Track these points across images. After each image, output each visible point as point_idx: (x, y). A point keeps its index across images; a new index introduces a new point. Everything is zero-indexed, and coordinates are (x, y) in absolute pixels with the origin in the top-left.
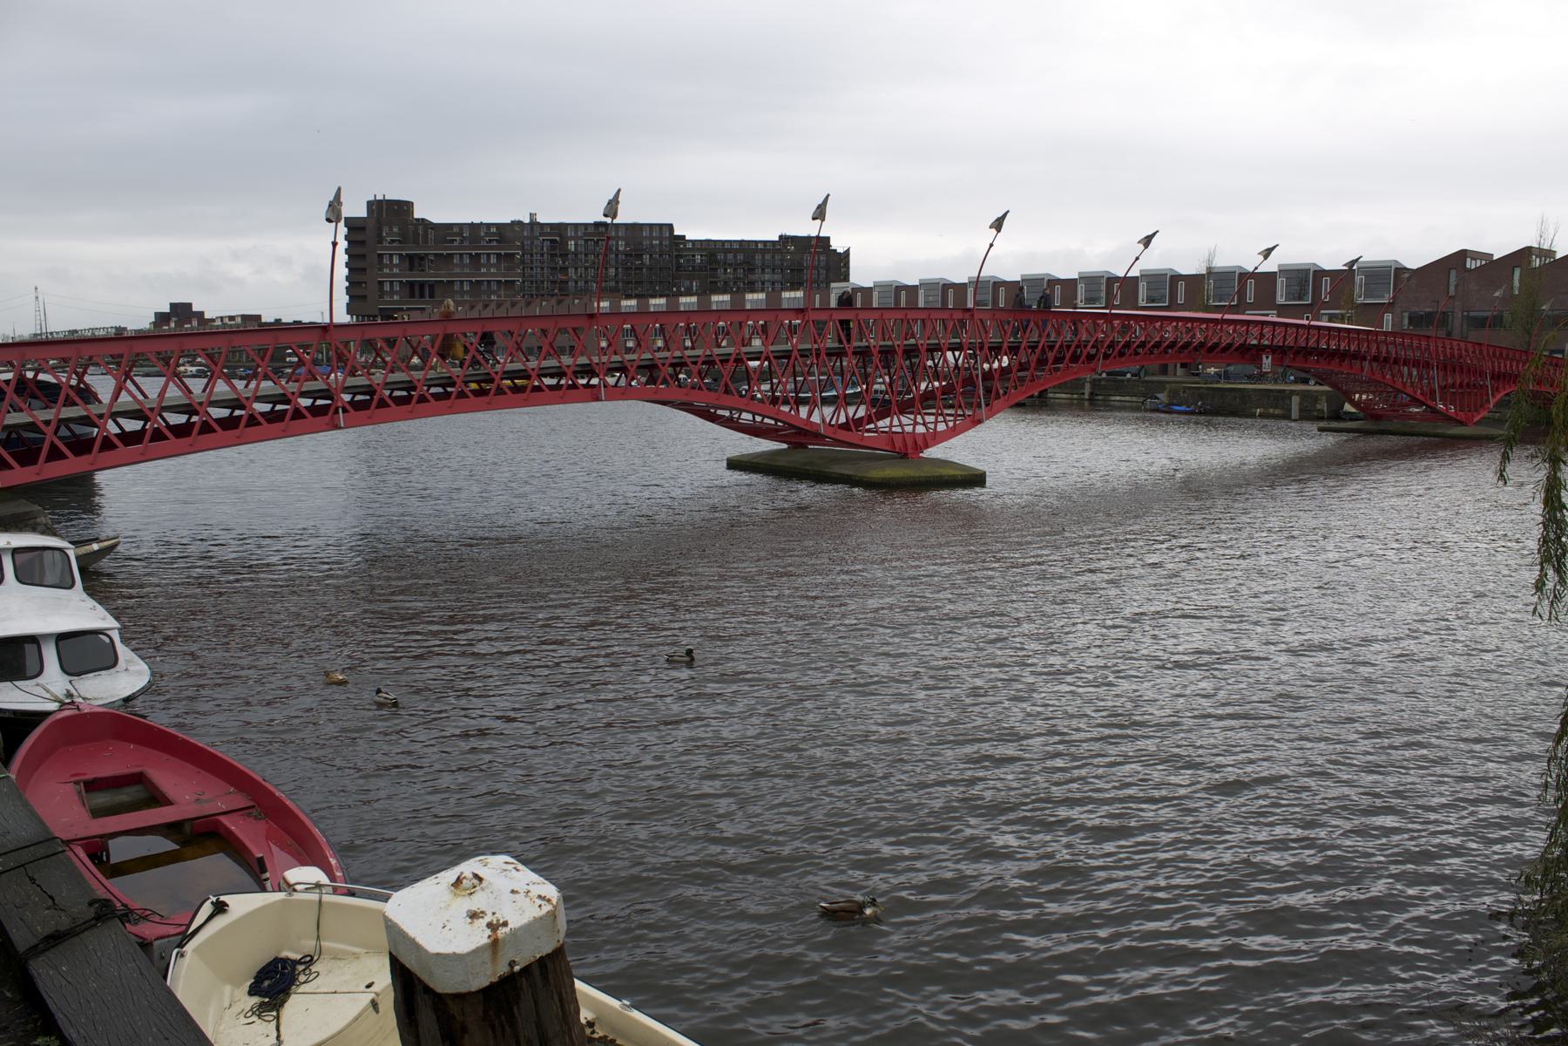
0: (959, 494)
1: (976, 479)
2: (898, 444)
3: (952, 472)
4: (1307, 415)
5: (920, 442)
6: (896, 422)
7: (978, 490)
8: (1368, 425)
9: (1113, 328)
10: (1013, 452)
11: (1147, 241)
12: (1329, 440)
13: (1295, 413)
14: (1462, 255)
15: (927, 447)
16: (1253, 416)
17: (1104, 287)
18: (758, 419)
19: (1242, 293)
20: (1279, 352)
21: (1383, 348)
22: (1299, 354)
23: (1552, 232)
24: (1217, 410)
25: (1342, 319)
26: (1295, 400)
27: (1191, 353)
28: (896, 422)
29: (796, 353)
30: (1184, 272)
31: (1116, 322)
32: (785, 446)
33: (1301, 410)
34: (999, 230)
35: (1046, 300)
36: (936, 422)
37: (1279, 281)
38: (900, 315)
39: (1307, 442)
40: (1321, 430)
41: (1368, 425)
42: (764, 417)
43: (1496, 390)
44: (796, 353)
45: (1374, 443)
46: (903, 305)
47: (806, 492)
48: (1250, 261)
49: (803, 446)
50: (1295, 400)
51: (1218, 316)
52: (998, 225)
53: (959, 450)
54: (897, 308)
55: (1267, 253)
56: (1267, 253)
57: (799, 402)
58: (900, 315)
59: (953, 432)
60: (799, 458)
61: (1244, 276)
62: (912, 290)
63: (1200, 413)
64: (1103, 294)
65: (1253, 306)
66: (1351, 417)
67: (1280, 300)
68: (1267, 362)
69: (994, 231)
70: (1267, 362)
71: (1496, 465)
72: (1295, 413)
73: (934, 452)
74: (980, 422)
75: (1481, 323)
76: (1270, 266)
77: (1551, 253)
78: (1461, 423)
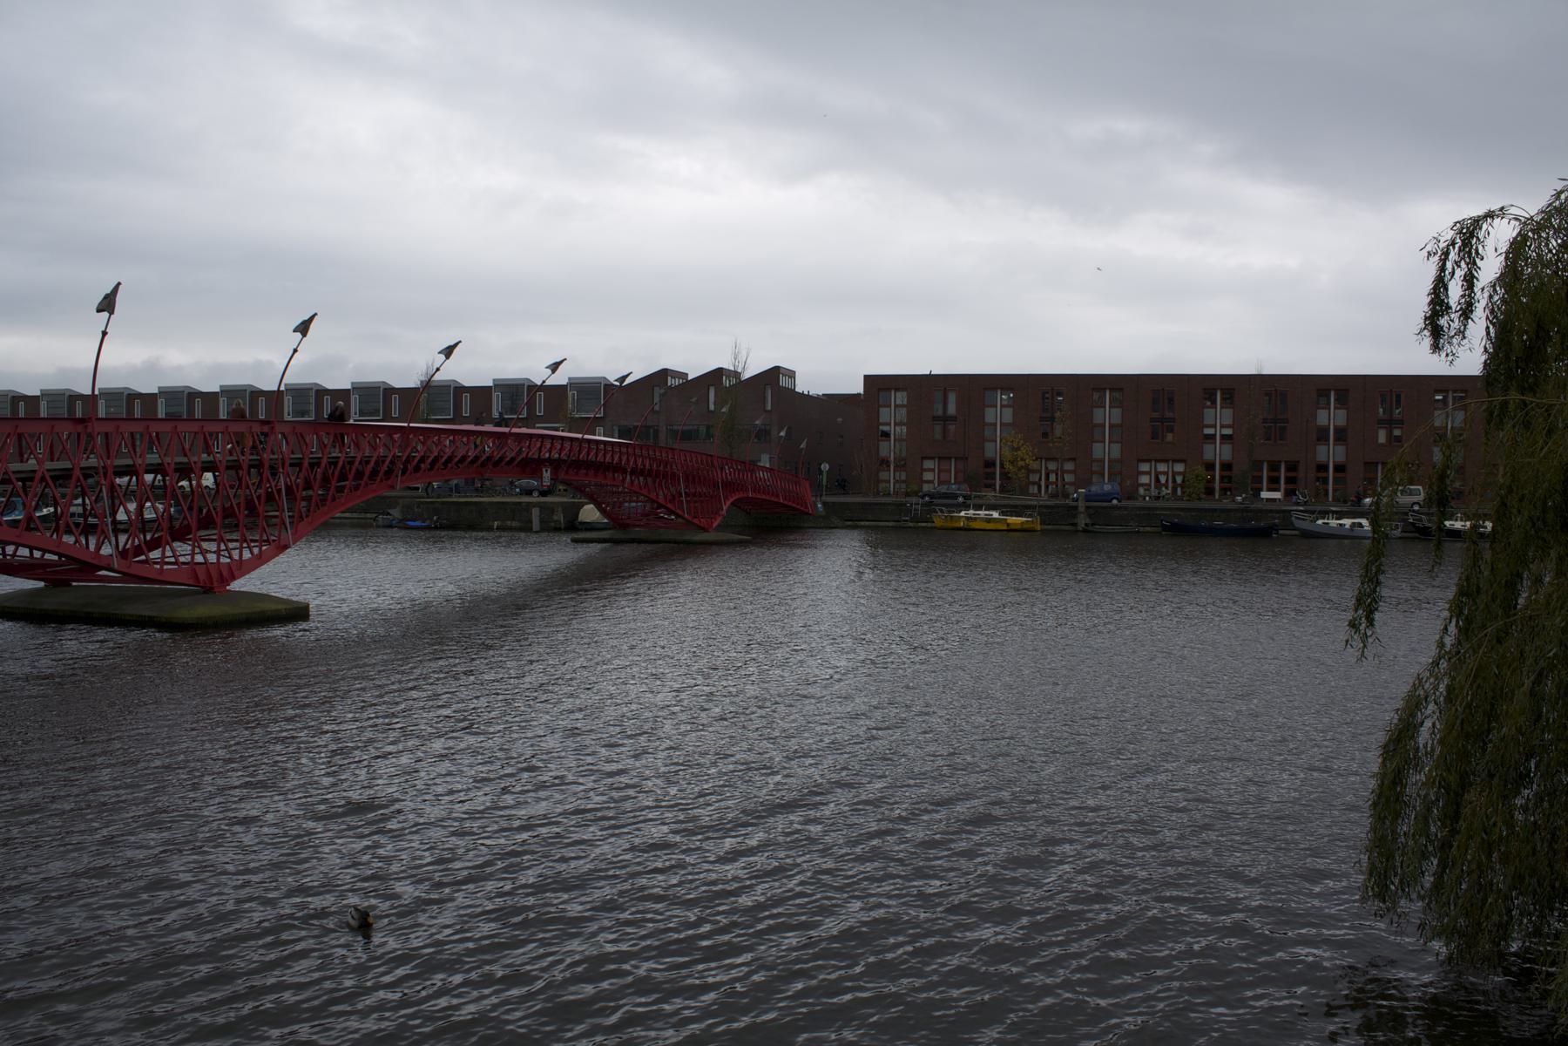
0: (278, 632)
1: (299, 613)
2: (202, 577)
3: (273, 607)
4: (550, 528)
5: (225, 573)
6: (169, 553)
7: (304, 625)
8: (619, 535)
9: (394, 441)
10: (339, 579)
11: (448, 352)
12: (583, 551)
13: (536, 525)
14: (664, 373)
15: (234, 578)
16: (490, 529)
17: (313, 400)
18: (37, 554)
19: (531, 404)
20: (556, 465)
21: (640, 462)
22: (580, 469)
23: (744, 353)
24: (506, 524)
25: (556, 429)
26: (535, 512)
27: (483, 467)
28: (169, 553)
29: (77, 473)
30: (397, 386)
31: (396, 436)
32: (41, 584)
33: (542, 521)
34: (304, 334)
35: (339, 416)
36: (241, 549)
37: (494, 395)
38: (195, 427)
39: (556, 555)
40: (575, 541)
41: (619, 535)
42: (44, 551)
43: (726, 498)
44: (77, 473)
45: (627, 551)
46: (137, 414)
47: (76, 643)
48: (537, 373)
49: (67, 583)
50: (535, 512)
51: (506, 430)
52: (303, 328)
53: (280, 576)
54: (192, 420)
55: (555, 367)
56: (555, 367)
57: (88, 530)
58: (195, 427)
59: (260, 560)
60: (60, 600)
61: (533, 388)
62: (32, 401)
63: (436, 528)
64: (313, 407)
65: (541, 420)
66: (590, 527)
67: (496, 415)
68: (547, 475)
69: (299, 335)
70: (547, 475)
71: (1348, 592)
72: (536, 525)
73: (236, 586)
74: (286, 547)
75: (687, 436)
76: (559, 379)
77: (736, 374)
78: (704, 530)
